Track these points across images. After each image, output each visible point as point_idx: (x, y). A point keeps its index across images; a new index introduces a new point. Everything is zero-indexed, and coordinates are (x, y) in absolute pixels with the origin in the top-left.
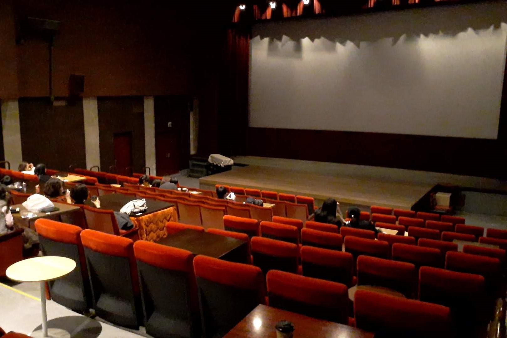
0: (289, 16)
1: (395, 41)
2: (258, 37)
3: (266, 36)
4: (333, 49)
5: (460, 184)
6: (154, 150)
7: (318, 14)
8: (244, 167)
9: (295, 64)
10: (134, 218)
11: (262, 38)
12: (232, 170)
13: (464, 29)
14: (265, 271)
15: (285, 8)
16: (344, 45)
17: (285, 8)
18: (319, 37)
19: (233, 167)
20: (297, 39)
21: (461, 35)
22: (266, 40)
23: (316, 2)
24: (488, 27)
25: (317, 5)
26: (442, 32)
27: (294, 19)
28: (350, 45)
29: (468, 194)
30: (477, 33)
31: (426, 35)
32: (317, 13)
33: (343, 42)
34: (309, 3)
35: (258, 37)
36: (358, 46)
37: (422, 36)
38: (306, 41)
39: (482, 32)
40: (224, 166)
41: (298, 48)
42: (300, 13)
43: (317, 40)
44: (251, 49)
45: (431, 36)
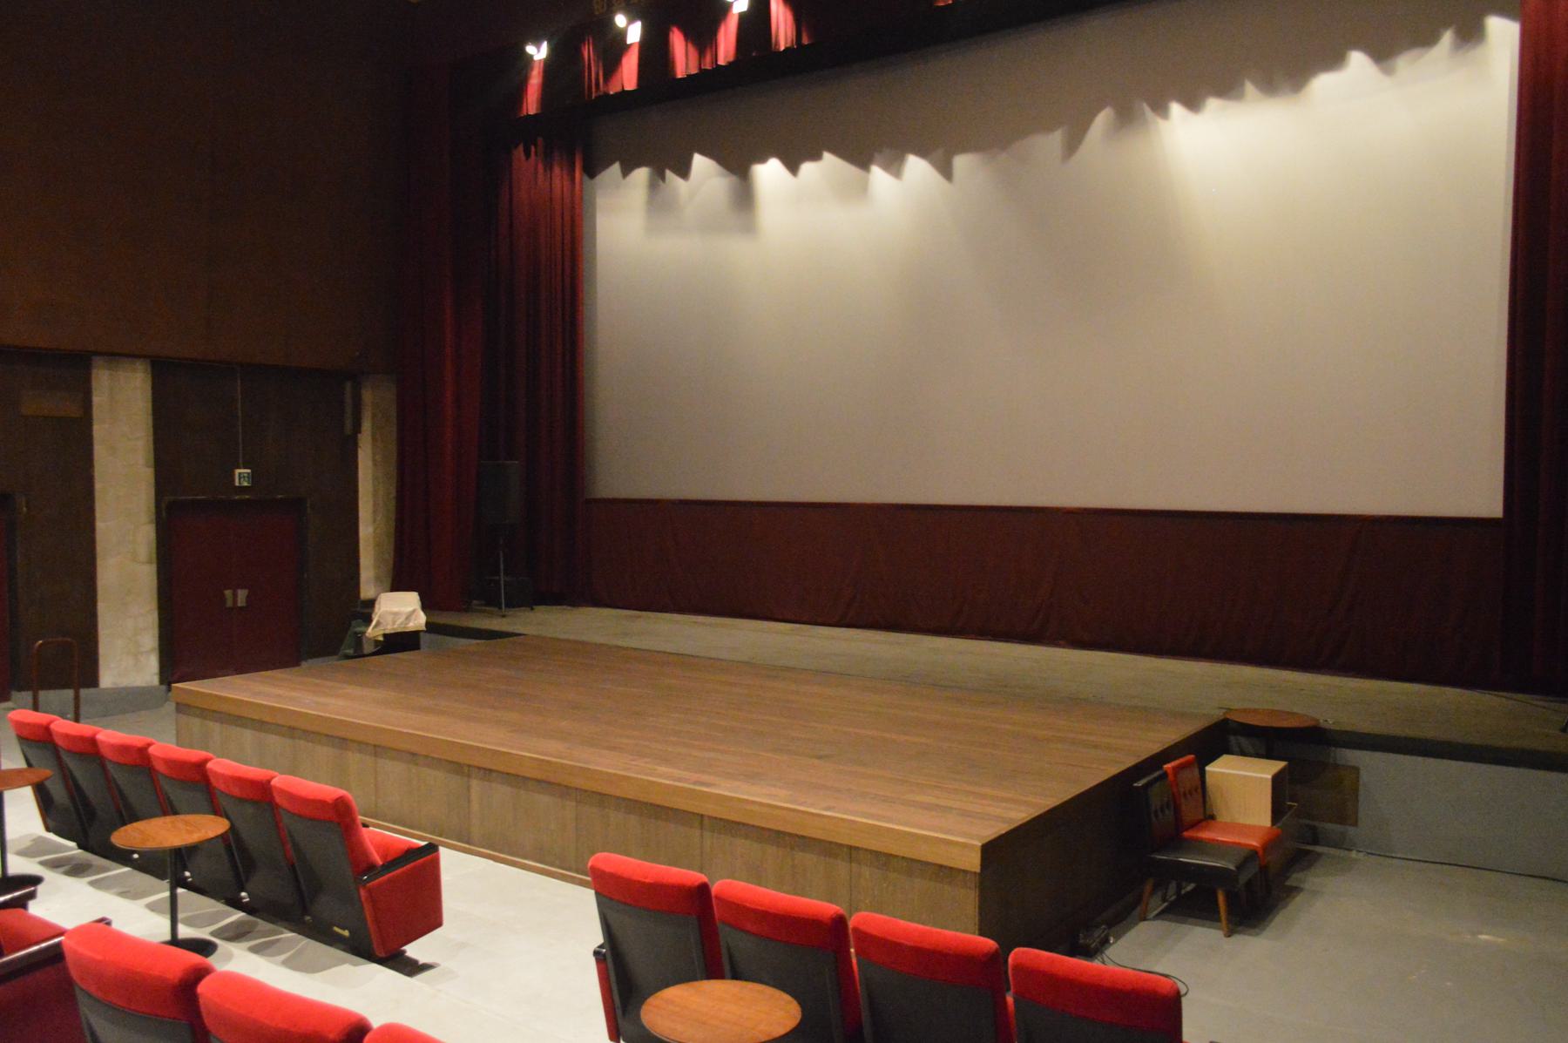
0: (694, 71)
1: (1073, 144)
2: (616, 168)
3: (639, 165)
4: (863, 190)
5: (1329, 718)
6: (146, 576)
7: (787, 49)
8: (493, 642)
9: (737, 251)
10: (206, 832)
11: (626, 171)
12: (422, 650)
13: (1333, 59)
14: (1007, 948)
15: (678, 45)
16: (897, 174)
17: (678, 45)
18: (816, 157)
19: (424, 639)
20: (738, 165)
21: (1324, 84)
22: (641, 174)
23: (779, 13)
24: (1427, 39)
25: (781, 18)
26: (1256, 83)
27: (710, 82)
28: (917, 167)
29: (1366, 761)
30: (1388, 71)
31: (1193, 103)
32: (782, 48)
33: (894, 167)
34: (748, 9)
35: (616, 168)
36: (946, 171)
37: (1176, 109)
38: (769, 173)
39: (1405, 63)
40: (385, 636)
41: (744, 197)
42: (726, 57)
43: (807, 168)
44: (593, 217)
45: (1213, 104)
